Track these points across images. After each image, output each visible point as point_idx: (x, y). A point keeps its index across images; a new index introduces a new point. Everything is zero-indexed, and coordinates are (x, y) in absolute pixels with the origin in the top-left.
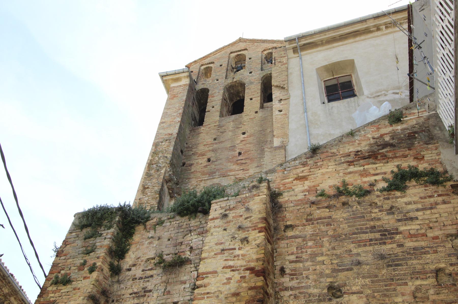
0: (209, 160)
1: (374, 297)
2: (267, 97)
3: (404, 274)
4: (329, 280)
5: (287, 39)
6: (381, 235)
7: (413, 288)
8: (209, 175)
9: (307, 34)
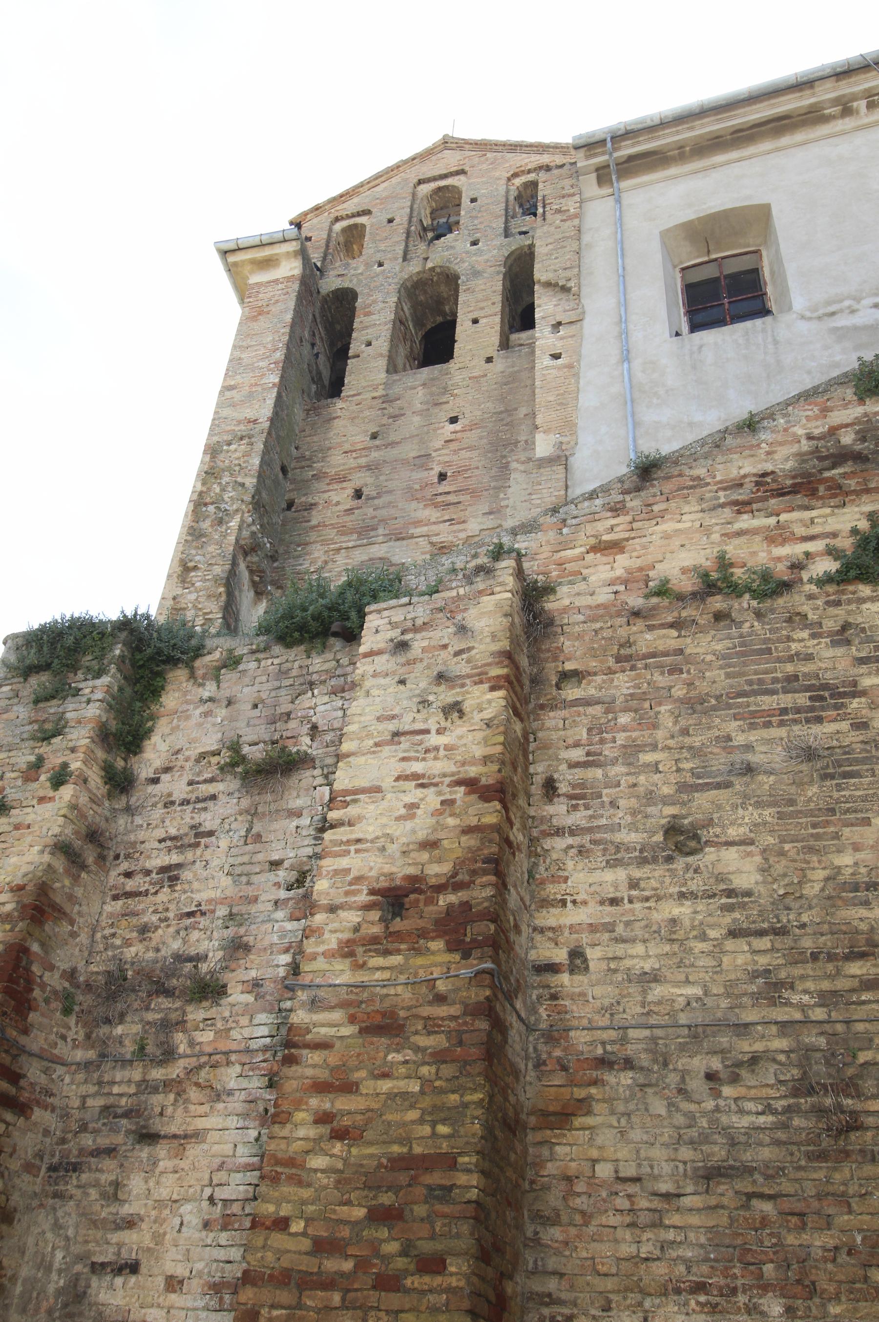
0: (358, 494)
1: (782, 853)
2: (520, 316)
5: (582, 142)
8: (359, 534)
9: (640, 126)
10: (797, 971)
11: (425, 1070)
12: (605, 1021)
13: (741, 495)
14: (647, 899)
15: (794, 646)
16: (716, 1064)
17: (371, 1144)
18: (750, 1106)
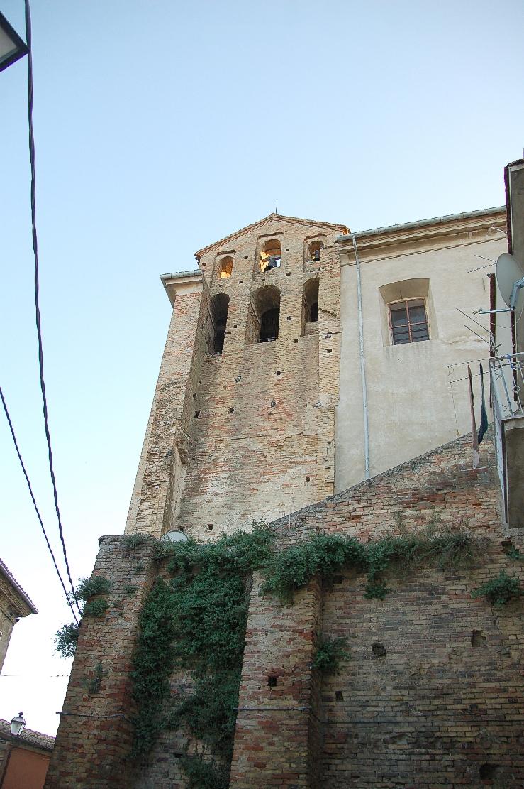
0: (232, 410)
1: (414, 657)
2: (312, 312)
3: (444, 637)
4: (376, 638)
6: (428, 594)
7: (450, 650)
10: (417, 703)
11: (286, 744)
12: (348, 720)
13: (406, 498)
14: (365, 673)
15: (424, 571)
16: (387, 736)
17: (269, 770)
18: (398, 752)
